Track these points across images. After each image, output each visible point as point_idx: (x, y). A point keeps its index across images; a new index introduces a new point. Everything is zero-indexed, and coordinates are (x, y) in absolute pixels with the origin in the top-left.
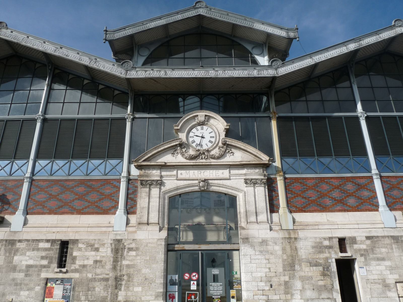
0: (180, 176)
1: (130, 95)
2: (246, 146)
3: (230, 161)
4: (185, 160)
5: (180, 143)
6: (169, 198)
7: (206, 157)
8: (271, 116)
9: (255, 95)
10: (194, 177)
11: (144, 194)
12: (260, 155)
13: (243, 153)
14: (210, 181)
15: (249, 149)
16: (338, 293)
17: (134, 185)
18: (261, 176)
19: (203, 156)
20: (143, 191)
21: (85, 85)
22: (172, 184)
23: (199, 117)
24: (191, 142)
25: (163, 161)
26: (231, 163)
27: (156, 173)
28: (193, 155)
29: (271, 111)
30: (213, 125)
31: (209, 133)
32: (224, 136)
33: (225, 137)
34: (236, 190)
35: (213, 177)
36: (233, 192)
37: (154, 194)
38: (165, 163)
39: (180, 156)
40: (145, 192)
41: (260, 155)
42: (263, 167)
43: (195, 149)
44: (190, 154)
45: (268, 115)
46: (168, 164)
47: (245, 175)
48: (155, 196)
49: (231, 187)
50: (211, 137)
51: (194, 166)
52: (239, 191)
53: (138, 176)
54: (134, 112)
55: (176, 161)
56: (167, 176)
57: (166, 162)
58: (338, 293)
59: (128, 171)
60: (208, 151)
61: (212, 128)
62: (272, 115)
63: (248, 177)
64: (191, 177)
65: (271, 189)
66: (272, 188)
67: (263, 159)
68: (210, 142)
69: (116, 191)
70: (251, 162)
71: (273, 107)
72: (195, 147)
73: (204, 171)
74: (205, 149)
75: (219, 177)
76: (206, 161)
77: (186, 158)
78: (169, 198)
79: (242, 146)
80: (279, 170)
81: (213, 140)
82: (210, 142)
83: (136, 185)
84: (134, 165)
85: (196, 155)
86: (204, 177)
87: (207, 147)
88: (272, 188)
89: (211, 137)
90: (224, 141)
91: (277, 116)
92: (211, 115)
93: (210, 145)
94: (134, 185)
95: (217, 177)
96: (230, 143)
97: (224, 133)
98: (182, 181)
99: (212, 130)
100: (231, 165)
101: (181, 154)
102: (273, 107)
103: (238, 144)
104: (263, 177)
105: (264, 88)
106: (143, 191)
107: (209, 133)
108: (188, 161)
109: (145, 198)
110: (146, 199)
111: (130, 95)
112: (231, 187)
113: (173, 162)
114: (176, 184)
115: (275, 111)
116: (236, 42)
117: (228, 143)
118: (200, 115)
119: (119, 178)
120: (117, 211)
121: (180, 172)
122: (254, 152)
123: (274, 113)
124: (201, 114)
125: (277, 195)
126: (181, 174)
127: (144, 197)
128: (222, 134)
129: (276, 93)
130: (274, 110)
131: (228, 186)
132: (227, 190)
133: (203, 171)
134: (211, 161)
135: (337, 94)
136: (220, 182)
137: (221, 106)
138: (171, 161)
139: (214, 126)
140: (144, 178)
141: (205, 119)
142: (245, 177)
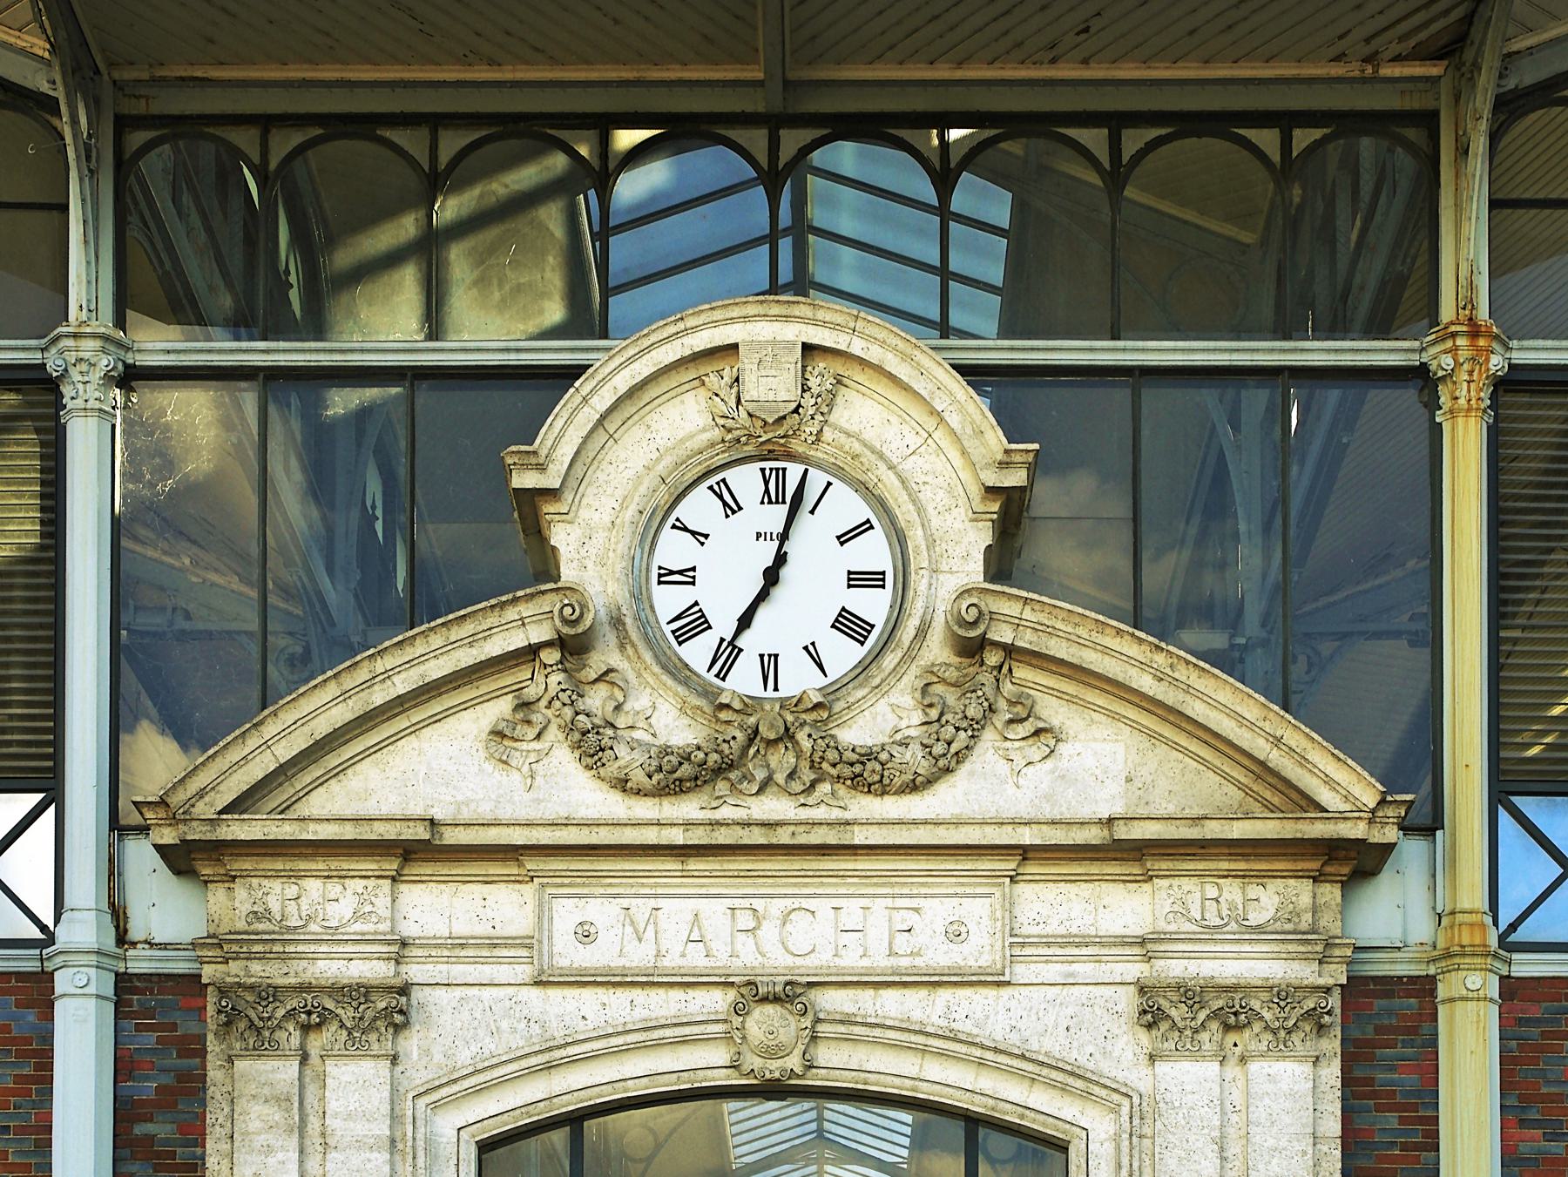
0: (569, 954)
1: (74, 122)
2: (1182, 673)
3: (1025, 812)
4: (615, 805)
5: (566, 630)
6: (486, 1147)
7: (808, 775)
9: (1303, 138)
10: (680, 956)
11: (257, 1109)
14: (831, 1001)
15: (1201, 696)
16: (124, 782)
18: (1296, 965)
19: (782, 760)
20: (252, 1089)
22: (504, 1025)
23: (747, 361)
24: (667, 629)
27: (358, 927)
29: (1447, 312)
30: (881, 456)
31: (843, 539)
32: (973, 571)
35: (865, 963)
36: (1040, 1099)
37: (349, 1117)
38: (432, 822)
39: (563, 759)
40: (266, 1091)
41: (1303, 761)
42: (1315, 880)
44: (660, 741)
45: (1414, 360)
46: (452, 837)
47: (1145, 945)
48: (360, 1129)
49: (1023, 1057)
50: (856, 579)
51: (694, 865)
53: (194, 945)
54: (130, 314)
56: (457, 945)
57: (438, 814)
58: (124, 782)
59: (112, 905)
60: (823, 708)
61: (864, 489)
62: (1454, 351)
63: (1175, 969)
64: (666, 962)
65: (1370, 1081)
66: (1381, 1076)
67: (1326, 797)
68: (849, 624)
69: (19, 1079)
70: (1213, 830)
71: (1463, 272)
72: (711, 677)
73: (789, 903)
74: (796, 692)
75: (919, 962)
76: (804, 814)
77: (622, 784)
78: (486, 1147)
80: (1459, 907)
81: (873, 606)
82: (849, 624)
83: (188, 1027)
84: (158, 847)
85: (714, 757)
86: (790, 961)
87: (822, 681)
88: (1381, 1076)
89: (856, 579)
90: (971, 616)
91: (1497, 363)
92: (857, 347)
93: (843, 654)
94: (174, 1027)
95: (904, 962)
96: (1026, 640)
97: (982, 537)
98: (589, 998)
100: (1025, 853)
102: (1463, 272)
103: (1106, 651)
104: (1305, 972)
105: (1397, 59)
106: (252, 1089)
107: (843, 539)
108: (645, 809)
109: (269, 1150)
110: (280, 1156)
111: (74, 124)
113: (505, 814)
116: (833, 81)
117: (1003, 634)
120: (1316, 140)
121: (567, 914)
123: (1475, 332)
124: (764, 331)
125: (1426, 1134)
126: (585, 935)
127: (262, 1139)
129: (1510, 107)
130: (1471, 304)
131: (996, 1050)
132: (987, 1082)
134: (848, 815)
136: (892, 1004)
138: (485, 811)
140: (256, 967)
142: (1136, 970)
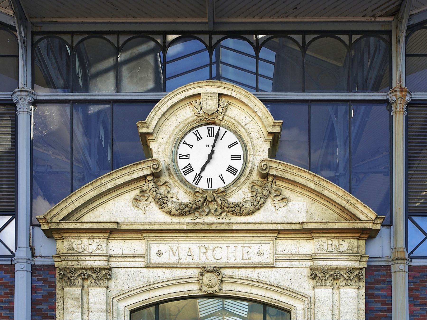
0: (155, 259)
1: (20, 33)
2: (322, 183)
3: (279, 220)
4: (168, 219)
5: (154, 171)
6: (132, 312)
7: (220, 211)
8: (392, 98)
9: (355, 37)
10: (185, 260)
11: (70, 301)
12: (355, 207)
13: (311, 201)
15: (327, 189)
17: (47, 279)
18: (353, 262)
19: (213, 206)
20: (68, 296)
21: (213, 46)
22: (137, 278)
23: (203, 98)
24: (182, 171)
25: (114, 220)
26: (280, 227)
27: (97, 252)
28: (187, 206)
29: (394, 85)
30: (240, 124)
31: (230, 147)
32: (265, 155)
33: (270, 156)
34: (290, 296)
35: (236, 261)
36: (283, 299)
37: (95, 303)
39: (153, 206)
41: (355, 207)
42: (358, 239)
43: (193, 188)
44: (180, 201)
45: (385, 98)
46: (123, 227)
47: (312, 257)
48: (98, 307)
49: (279, 287)
50: (233, 158)
52: (296, 298)
55: (145, 221)
56: (124, 257)
57: (119, 221)
59: (31, 246)
61: (235, 133)
62: (396, 95)
63: (320, 263)
64: (181, 261)
66: (376, 293)
67: (361, 216)
68: (231, 170)
69: (5, 293)
70: (330, 225)
71: (399, 74)
72: (194, 184)
75: (250, 261)
76: (219, 221)
77: (169, 213)
78: (132, 312)
79: (311, 181)
81: (238, 165)
82: (231, 170)
83: (51, 279)
86: (215, 261)
87: (224, 185)
88: (376, 293)
89: (233, 158)
91: (408, 99)
92: (233, 94)
93: (230, 178)
94: (47, 279)
95: (246, 261)
96: (279, 174)
97: (267, 146)
99: (234, 139)
101: (157, 203)
102: (399, 74)
103: (301, 177)
104: (356, 264)
105: (380, 16)
106: (68, 296)
107: (230, 147)
108: (176, 220)
109: (73, 312)
110: (76, 314)
111: (20, 33)
112: (279, 287)
113: (138, 221)
114: (146, 280)
115: (404, 85)
117: (273, 172)
118: (206, 94)
119: (9, 263)
121: (154, 248)
122: (341, 197)
123: (402, 90)
124: (208, 90)
125: (388, 308)
126: (159, 254)
127: (71, 310)
128: (261, 149)
129: (411, 29)
130: (401, 83)
131: (271, 285)
132: (269, 294)
133: (211, 246)
134: (231, 221)
135: (273, 4)
136: (243, 273)
137: (396, 93)
138: (132, 220)
139: (243, 127)
140: (70, 263)
141: (219, 106)
142: (309, 263)
